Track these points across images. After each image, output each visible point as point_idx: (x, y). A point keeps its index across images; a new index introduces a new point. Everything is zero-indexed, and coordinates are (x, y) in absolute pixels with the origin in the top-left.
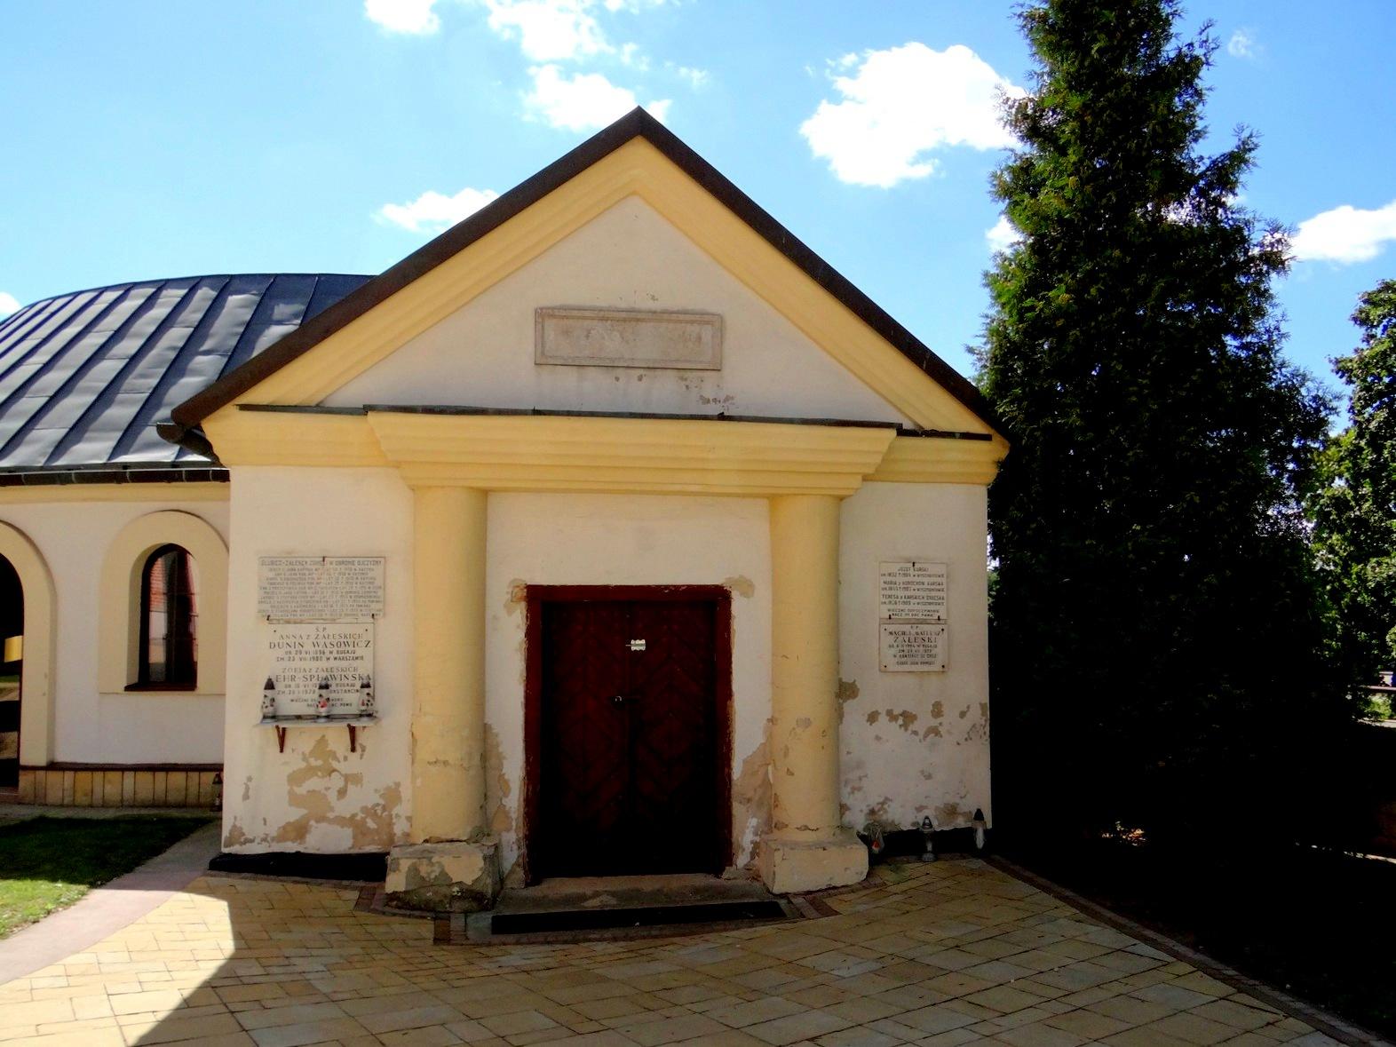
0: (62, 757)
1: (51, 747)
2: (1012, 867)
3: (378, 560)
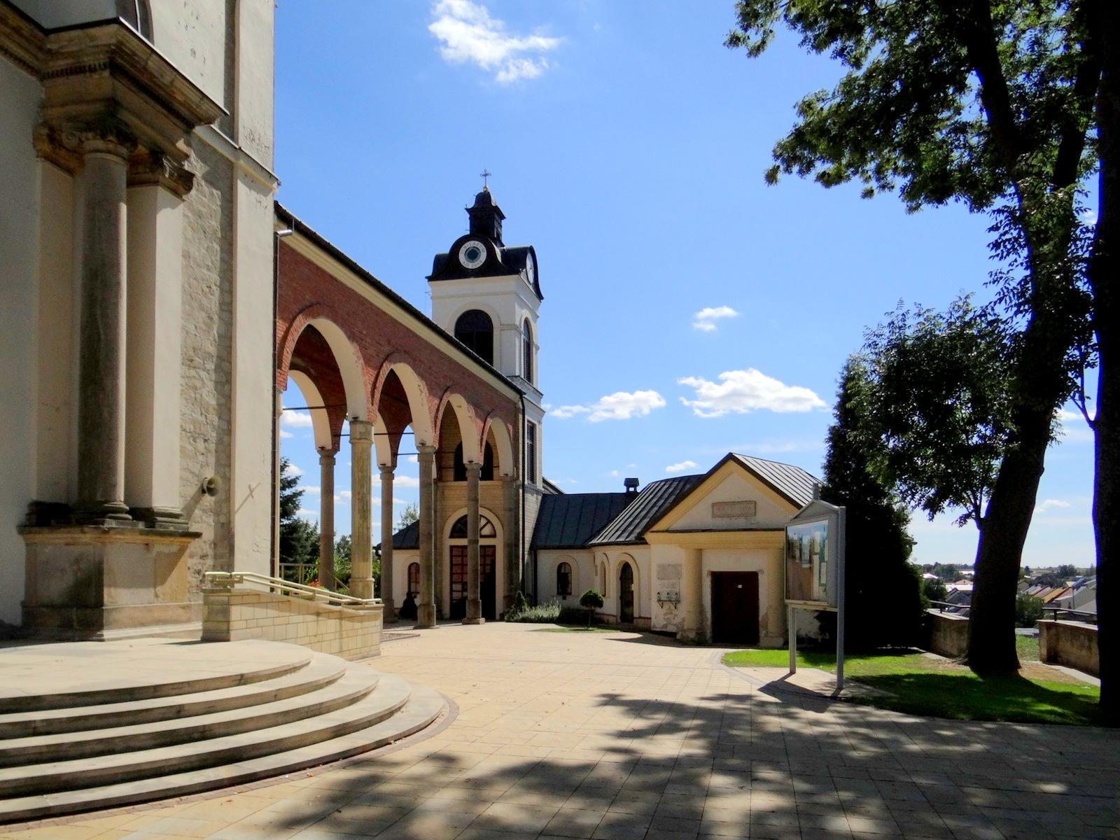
0: (642, 616)
1: (640, 613)
2: (1020, 700)
3: (681, 565)
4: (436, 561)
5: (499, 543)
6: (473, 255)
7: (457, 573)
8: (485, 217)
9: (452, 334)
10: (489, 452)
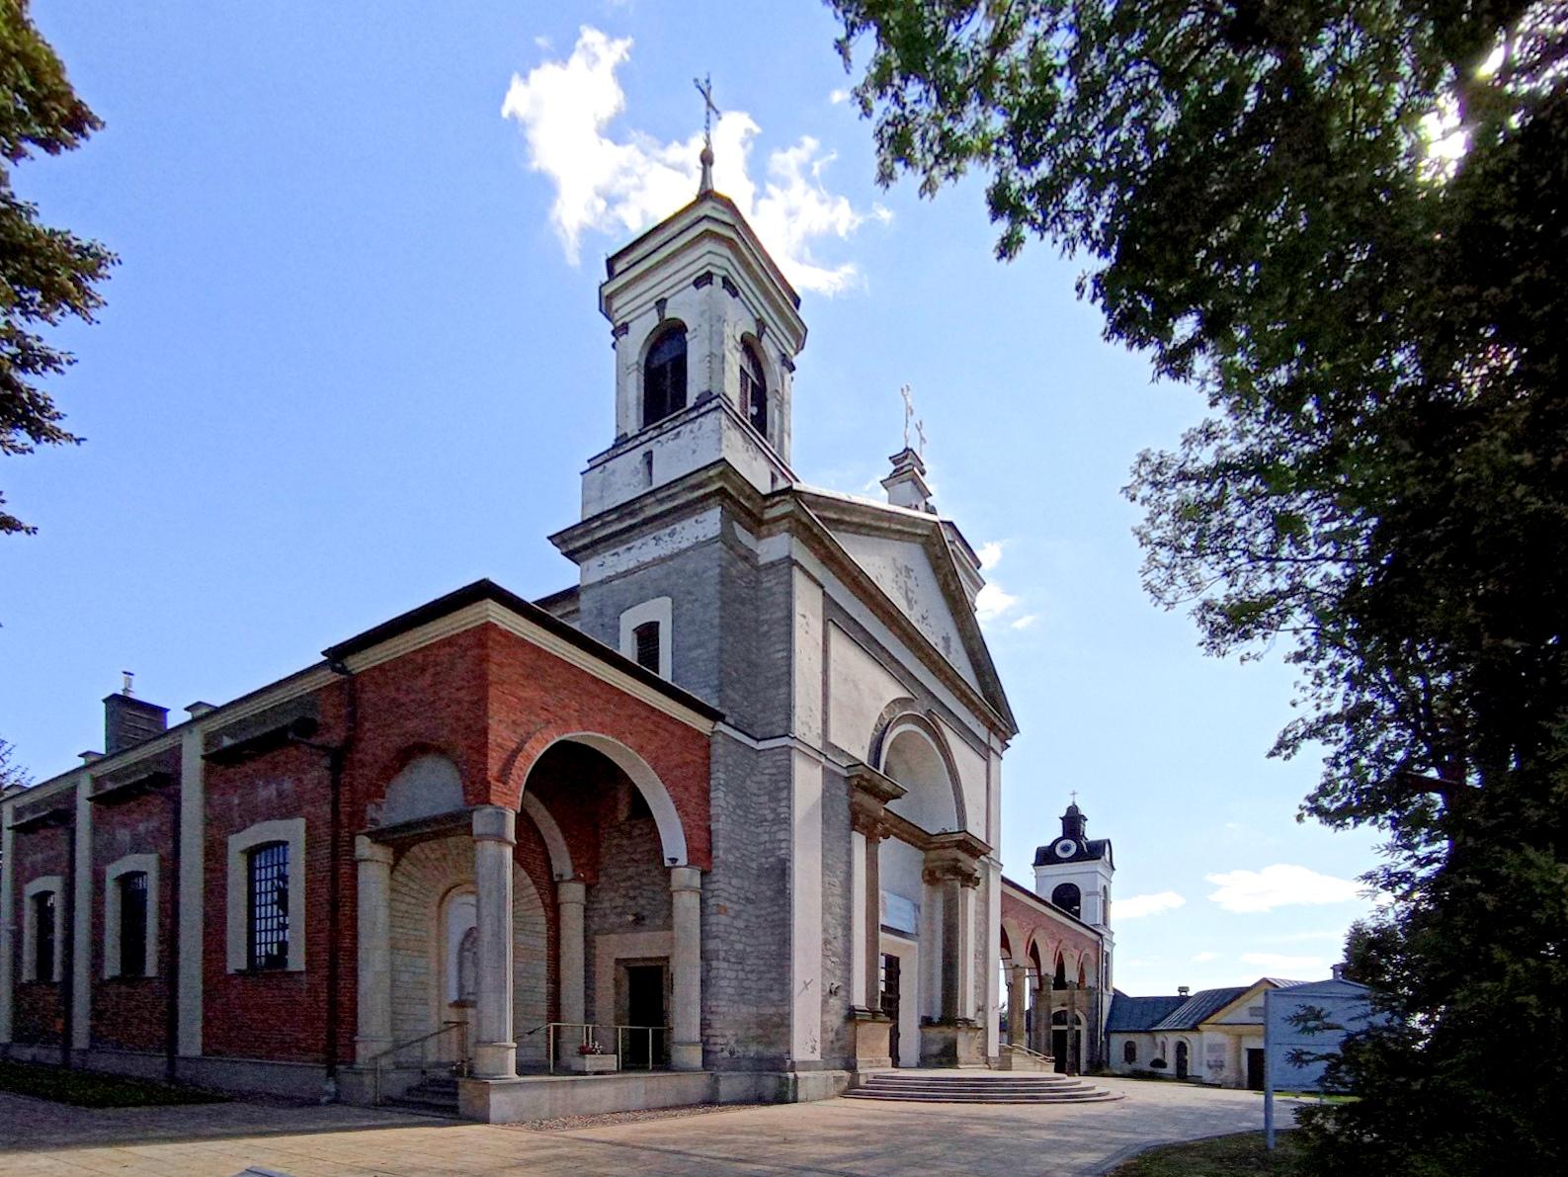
4: (128, 777)
5: (1083, 1029)
6: (1066, 849)
7: (1268, 1106)
8: (1073, 822)
9: (1050, 901)
10: (1061, 968)
